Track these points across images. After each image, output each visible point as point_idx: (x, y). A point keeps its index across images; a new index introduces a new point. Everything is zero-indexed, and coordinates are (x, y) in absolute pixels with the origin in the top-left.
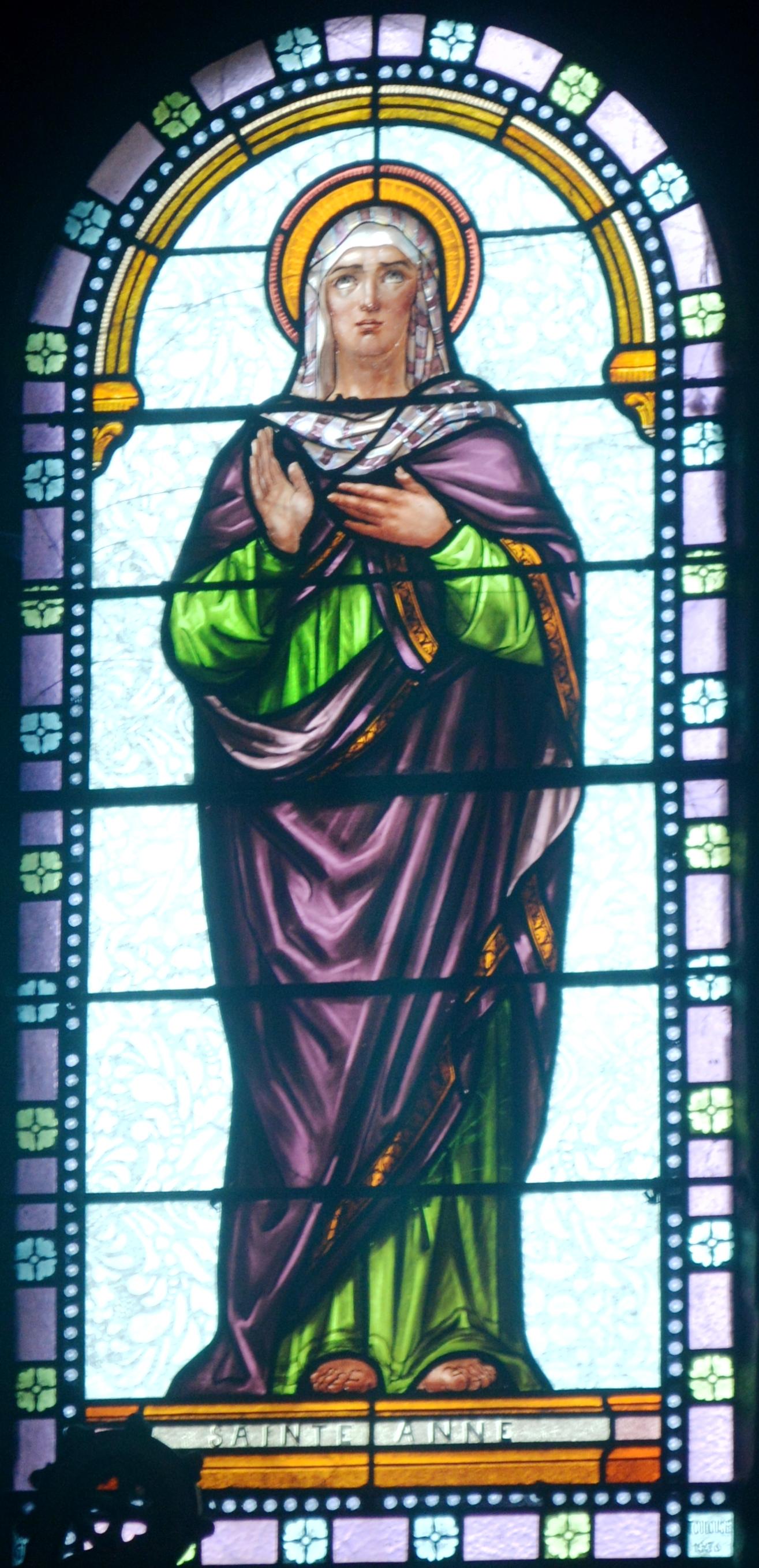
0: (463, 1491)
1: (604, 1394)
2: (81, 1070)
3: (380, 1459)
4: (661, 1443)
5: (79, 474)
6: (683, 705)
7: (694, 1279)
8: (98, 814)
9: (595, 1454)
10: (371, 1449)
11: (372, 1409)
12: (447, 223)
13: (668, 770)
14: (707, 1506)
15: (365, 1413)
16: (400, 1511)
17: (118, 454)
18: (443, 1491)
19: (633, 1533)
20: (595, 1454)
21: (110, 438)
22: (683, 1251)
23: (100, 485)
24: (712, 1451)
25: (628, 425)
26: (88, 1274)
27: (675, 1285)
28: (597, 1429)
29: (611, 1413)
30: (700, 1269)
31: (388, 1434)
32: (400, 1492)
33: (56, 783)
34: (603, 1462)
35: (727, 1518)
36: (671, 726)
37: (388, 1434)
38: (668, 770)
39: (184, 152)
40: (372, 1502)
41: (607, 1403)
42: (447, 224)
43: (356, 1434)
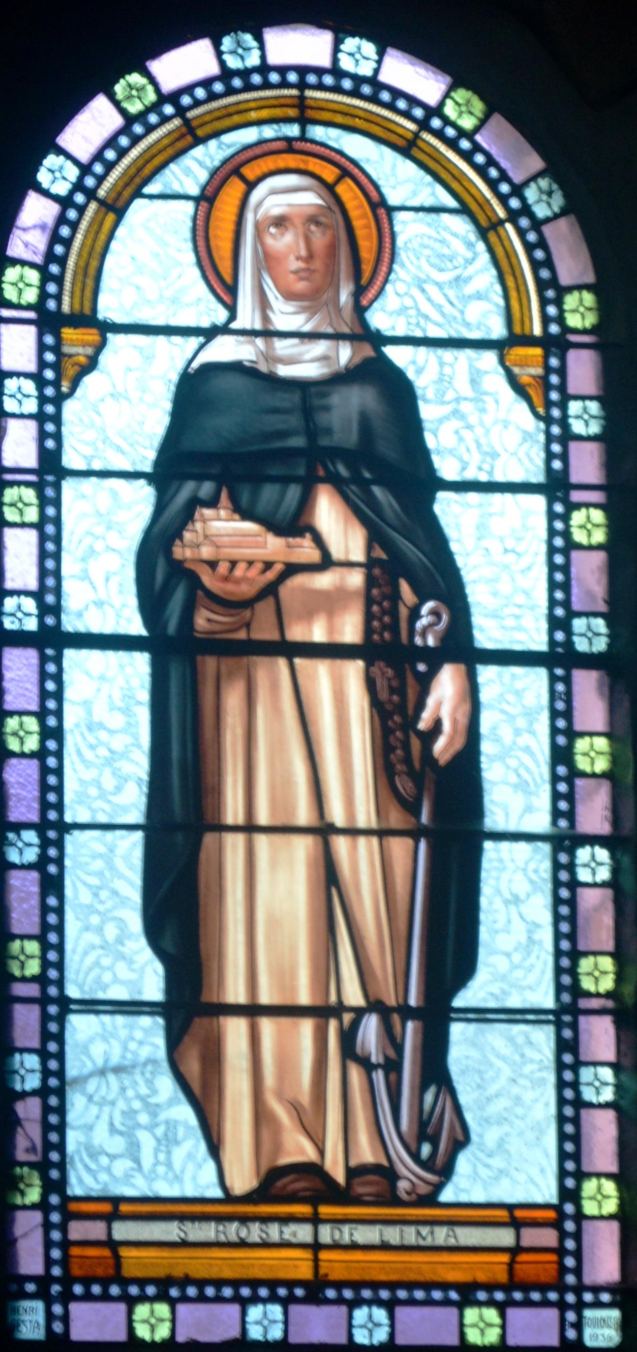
0: (393, 1286)
1: (510, 1208)
2: (60, 911)
3: (324, 1255)
4: (561, 1251)
5: (49, 391)
6: (576, 754)
7: (575, 555)
8: (70, 654)
9: (505, 1258)
10: (316, 1247)
11: (316, 1213)
12: (367, 227)
13: (560, 659)
14: (598, 1304)
15: (310, 1216)
16: (340, 1301)
17: (87, 380)
18: (375, 1286)
19: (537, 1325)
20: (505, 1258)
21: (77, 368)
22: (566, 534)
23: (69, 408)
24: (605, 1262)
25: (524, 406)
26: (36, 793)
27: (568, 1076)
28: (505, 1237)
29: (516, 1224)
30: (579, 547)
31: (326, 1234)
32: (339, 1285)
33: (31, 625)
34: (511, 1265)
35: (615, 1314)
36: (565, 804)
37: (326, 1234)
38: (560, 659)
39: (138, 129)
40: (315, 1291)
41: (515, 1216)
42: (369, 237)
43: (303, 1233)
